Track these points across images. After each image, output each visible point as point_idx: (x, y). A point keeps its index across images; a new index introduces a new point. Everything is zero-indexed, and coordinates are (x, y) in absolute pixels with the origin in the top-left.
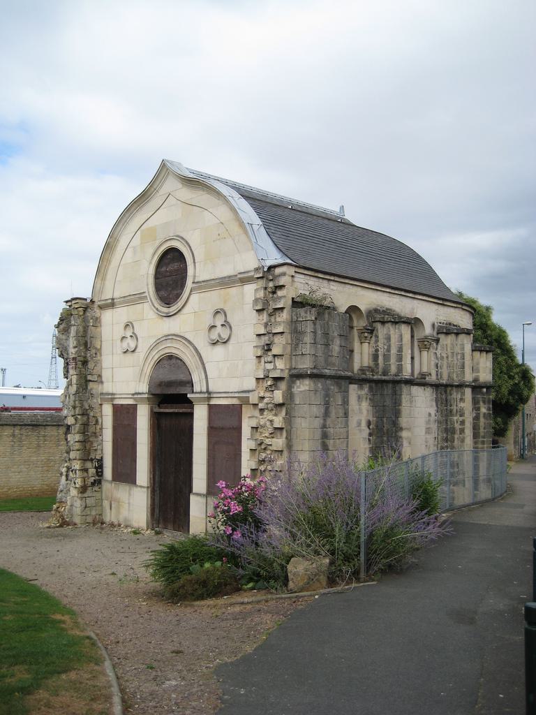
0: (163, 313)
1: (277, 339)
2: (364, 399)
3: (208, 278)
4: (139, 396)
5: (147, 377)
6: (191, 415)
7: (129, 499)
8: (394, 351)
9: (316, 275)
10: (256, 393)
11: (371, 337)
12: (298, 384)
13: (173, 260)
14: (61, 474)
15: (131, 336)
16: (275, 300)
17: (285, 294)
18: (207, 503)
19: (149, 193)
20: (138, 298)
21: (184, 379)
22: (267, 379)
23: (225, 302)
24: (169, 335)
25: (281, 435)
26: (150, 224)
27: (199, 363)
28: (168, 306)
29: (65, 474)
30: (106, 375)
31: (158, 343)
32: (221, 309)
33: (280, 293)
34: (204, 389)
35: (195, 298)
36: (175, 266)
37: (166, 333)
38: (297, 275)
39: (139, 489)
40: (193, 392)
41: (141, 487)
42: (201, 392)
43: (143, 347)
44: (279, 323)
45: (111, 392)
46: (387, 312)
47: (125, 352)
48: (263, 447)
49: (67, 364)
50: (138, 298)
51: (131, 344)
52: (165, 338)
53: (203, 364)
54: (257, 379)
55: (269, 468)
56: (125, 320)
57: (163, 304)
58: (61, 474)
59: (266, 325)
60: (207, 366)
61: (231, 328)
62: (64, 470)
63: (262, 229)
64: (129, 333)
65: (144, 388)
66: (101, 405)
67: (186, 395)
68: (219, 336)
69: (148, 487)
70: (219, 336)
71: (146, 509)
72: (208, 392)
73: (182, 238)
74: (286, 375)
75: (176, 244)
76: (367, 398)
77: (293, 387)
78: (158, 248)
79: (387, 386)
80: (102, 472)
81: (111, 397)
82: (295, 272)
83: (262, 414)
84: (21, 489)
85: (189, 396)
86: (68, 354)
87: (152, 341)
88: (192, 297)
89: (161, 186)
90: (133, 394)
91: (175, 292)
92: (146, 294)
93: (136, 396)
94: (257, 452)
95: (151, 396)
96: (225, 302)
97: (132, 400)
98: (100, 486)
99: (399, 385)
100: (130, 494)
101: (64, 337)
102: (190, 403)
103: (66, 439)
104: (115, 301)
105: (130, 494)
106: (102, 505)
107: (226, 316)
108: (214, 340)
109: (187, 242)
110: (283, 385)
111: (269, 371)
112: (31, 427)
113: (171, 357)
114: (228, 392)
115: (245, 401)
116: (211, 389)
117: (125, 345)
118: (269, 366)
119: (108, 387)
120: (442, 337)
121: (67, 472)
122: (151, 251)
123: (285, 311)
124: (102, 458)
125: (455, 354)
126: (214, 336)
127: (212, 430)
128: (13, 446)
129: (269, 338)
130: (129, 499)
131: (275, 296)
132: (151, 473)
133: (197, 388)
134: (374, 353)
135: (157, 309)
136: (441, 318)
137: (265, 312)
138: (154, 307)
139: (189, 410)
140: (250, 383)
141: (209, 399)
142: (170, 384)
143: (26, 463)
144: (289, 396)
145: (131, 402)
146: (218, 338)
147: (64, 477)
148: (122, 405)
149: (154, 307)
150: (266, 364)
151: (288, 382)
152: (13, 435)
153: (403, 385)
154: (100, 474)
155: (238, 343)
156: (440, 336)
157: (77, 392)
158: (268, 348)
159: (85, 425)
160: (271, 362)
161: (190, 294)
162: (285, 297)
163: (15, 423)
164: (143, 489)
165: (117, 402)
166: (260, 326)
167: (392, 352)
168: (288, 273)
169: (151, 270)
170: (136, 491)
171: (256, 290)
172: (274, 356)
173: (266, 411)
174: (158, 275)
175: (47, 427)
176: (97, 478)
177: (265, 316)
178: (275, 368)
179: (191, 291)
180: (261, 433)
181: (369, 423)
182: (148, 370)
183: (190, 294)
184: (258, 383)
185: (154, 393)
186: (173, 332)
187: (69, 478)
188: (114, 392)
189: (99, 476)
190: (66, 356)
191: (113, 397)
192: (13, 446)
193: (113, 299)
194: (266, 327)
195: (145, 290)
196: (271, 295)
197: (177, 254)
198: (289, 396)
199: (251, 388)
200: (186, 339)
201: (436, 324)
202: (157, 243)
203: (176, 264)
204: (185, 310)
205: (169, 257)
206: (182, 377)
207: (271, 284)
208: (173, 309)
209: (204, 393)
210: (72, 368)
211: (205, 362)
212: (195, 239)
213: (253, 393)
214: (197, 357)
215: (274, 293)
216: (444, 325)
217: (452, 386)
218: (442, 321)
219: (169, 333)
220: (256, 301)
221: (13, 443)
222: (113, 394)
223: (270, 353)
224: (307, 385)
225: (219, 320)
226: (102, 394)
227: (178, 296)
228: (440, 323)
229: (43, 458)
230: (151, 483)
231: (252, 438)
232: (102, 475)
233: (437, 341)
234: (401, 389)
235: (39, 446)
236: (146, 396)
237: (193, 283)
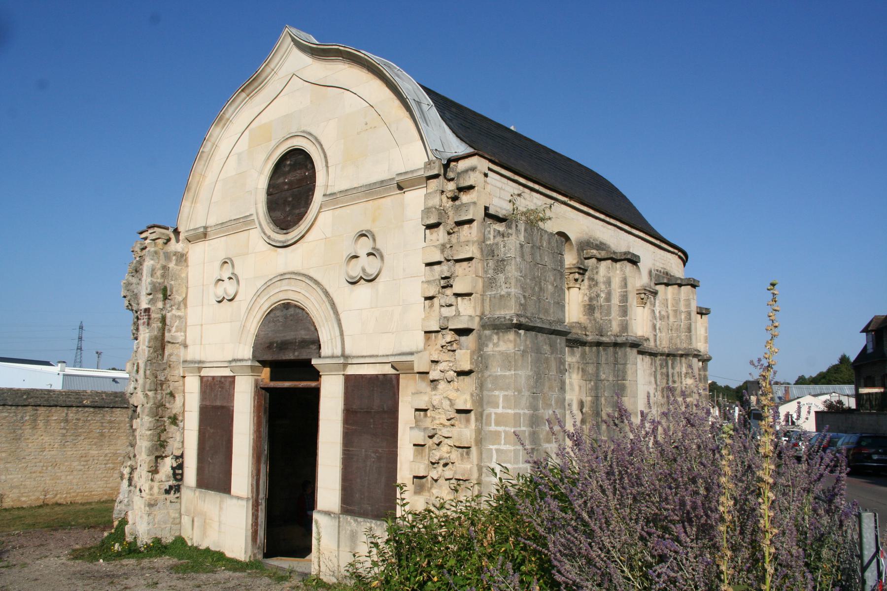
0: (280, 242)
1: (460, 268)
2: (576, 370)
3: (346, 188)
4: (239, 364)
5: (204, 193)
6: (316, 392)
7: (220, 516)
8: (615, 300)
9: (517, 178)
10: (426, 353)
11: (583, 281)
12: (495, 341)
13: (293, 167)
14: (122, 477)
15: (230, 278)
16: (457, 209)
17: (475, 200)
18: (339, 526)
19: (264, 76)
20: (242, 223)
21: (307, 337)
22: (444, 332)
23: (374, 221)
24: (285, 274)
25: (468, 421)
26: (263, 119)
27: (331, 312)
28: (285, 231)
29: (127, 476)
30: (192, 335)
31: (268, 285)
32: (367, 231)
33: (465, 198)
34: (338, 352)
35: (326, 218)
36: (298, 174)
37: (282, 271)
38: (490, 174)
39: (235, 501)
40: (320, 357)
41: (238, 498)
42: (333, 357)
43: (246, 294)
44: (467, 243)
45: (198, 358)
46: (601, 246)
47: (219, 302)
48: (436, 440)
49: (138, 318)
50: (242, 223)
51: (229, 288)
52: (279, 278)
53: (336, 313)
54: (426, 332)
55: (448, 474)
56: (222, 256)
57: (278, 230)
58: (122, 477)
59: (443, 248)
60: (342, 316)
61: (382, 257)
62: (126, 471)
63: (434, 110)
64: (226, 275)
65: (246, 351)
66: (184, 377)
67: (310, 360)
68: (364, 270)
69: (248, 499)
70: (364, 270)
71: (244, 532)
72: (344, 356)
73: (310, 134)
74: (475, 325)
75: (300, 143)
76: (579, 368)
77: (487, 346)
78: (272, 152)
79: (604, 350)
80: (182, 475)
81: (199, 365)
82: (490, 169)
83: (435, 388)
84: (73, 494)
85: (314, 362)
86: (138, 304)
87: (260, 283)
88: (321, 215)
89: (282, 65)
90: (230, 362)
91: (297, 211)
92: (254, 217)
93: (234, 364)
94: (426, 448)
95: (257, 364)
96: (374, 221)
97: (228, 369)
98: (178, 495)
99: (623, 349)
100: (221, 508)
101: (134, 280)
102: (315, 375)
103: (132, 426)
104: (209, 230)
105: (221, 508)
106: (180, 523)
107: (374, 240)
108: (353, 278)
109: (316, 139)
110: (469, 341)
111: (447, 319)
112: (92, 410)
113: (287, 306)
114: (377, 356)
115: (402, 368)
116: (348, 352)
117: (220, 291)
118: (446, 312)
119: (193, 353)
120: (660, 288)
121: (131, 473)
122: (263, 157)
123: (475, 223)
124: (182, 454)
125: (678, 313)
126: (355, 270)
127: (350, 415)
128: (64, 435)
129: (450, 268)
130: (220, 516)
131: (457, 203)
132: (253, 477)
133: (325, 350)
134: (587, 303)
135: (269, 237)
136: (658, 264)
137: (441, 227)
138: (265, 234)
139: (313, 384)
140: (417, 340)
141: (345, 365)
142: (284, 346)
143: (83, 459)
144: (481, 358)
145: (227, 372)
146: (362, 274)
147: (125, 483)
148: (213, 377)
149: (265, 234)
150: (443, 309)
151: (480, 337)
152: (66, 421)
153: (628, 349)
154: (179, 477)
155: (394, 280)
156: (658, 288)
157: (149, 361)
158: (447, 282)
159: (160, 407)
160: (451, 305)
161: (319, 212)
162: (475, 203)
163: (70, 404)
164: (240, 502)
165: (205, 373)
166: (434, 249)
167: (613, 302)
168: (479, 168)
169: (262, 182)
170: (229, 503)
171: (427, 196)
172: (457, 295)
173: (442, 383)
174: (273, 190)
175: (114, 410)
176: (174, 482)
177: (440, 235)
178: (458, 314)
179: (321, 208)
180: (433, 419)
181: (581, 405)
182: (253, 326)
183: (319, 212)
184: (427, 339)
185: (261, 359)
186: (291, 269)
187: (133, 483)
188: (203, 359)
189: (176, 479)
190: (135, 307)
191: (200, 365)
192: (64, 435)
193: (205, 228)
194: (442, 251)
195: (253, 211)
196: (450, 203)
197: (300, 154)
198: (481, 358)
199: (414, 349)
200: (311, 278)
201: (653, 271)
202: (274, 143)
203: (299, 172)
204: (309, 237)
205: (288, 162)
206: (303, 334)
207: (451, 186)
208: (294, 234)
209: (337, 357)
210: (144, 323)
211: (340, 311)
212: (328, 134)
213: (420, 354)
214: (327, 303)
215: (455, 199)
216: (662, 274)
217: (674, 355)
218: (660, 269)
219: (285, 271)
220: (427, 211)
221: (64, 431)
222: (200, 362)
223: (449, 291)
224: (511, 341)
225: (365, 246)
226: (185, 362)
227: (300, 217)
228: (657, 271)
229: (107, 451)
230: (252, 492)
231: (418, 424)
232: (181, 479)
233: (655, 293)
234: (625, 355)
235: (102, 435)
236: (249, 363)
237: (324, 195)
